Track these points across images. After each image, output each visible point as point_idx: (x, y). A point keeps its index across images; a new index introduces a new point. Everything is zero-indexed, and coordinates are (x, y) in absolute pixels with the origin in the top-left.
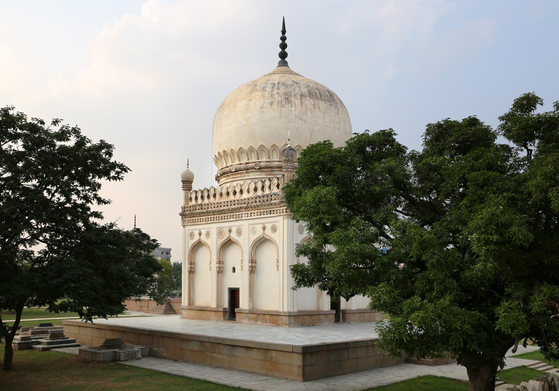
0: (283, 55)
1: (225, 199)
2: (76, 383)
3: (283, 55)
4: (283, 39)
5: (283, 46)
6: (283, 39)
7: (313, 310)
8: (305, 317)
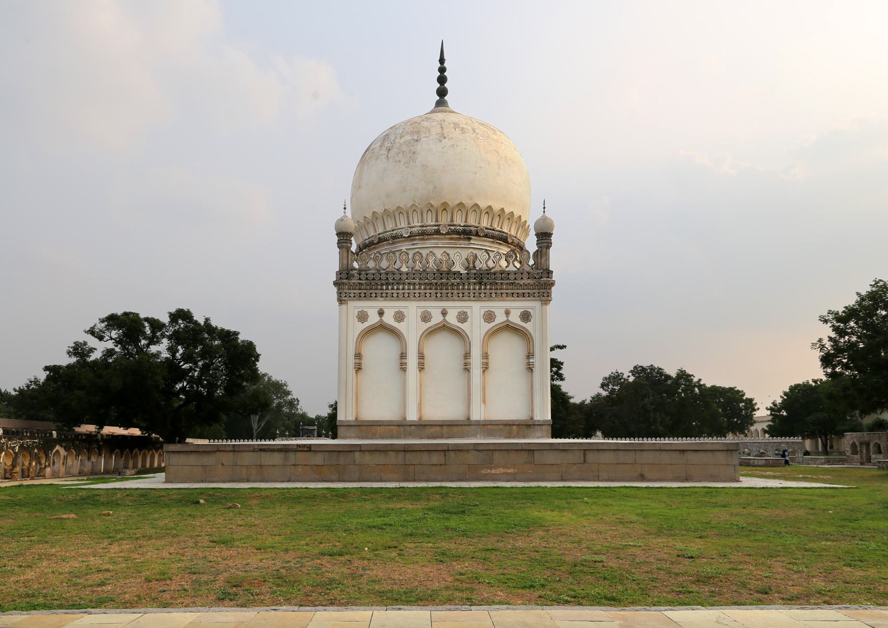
0: (442, 92)
1: (521, 291)
2: (493, 471)
3: (442, 92)
4: (442, 70)
5: (442, 80)
6: (442, 70)
7: (384, 419)
8: (392, 427)
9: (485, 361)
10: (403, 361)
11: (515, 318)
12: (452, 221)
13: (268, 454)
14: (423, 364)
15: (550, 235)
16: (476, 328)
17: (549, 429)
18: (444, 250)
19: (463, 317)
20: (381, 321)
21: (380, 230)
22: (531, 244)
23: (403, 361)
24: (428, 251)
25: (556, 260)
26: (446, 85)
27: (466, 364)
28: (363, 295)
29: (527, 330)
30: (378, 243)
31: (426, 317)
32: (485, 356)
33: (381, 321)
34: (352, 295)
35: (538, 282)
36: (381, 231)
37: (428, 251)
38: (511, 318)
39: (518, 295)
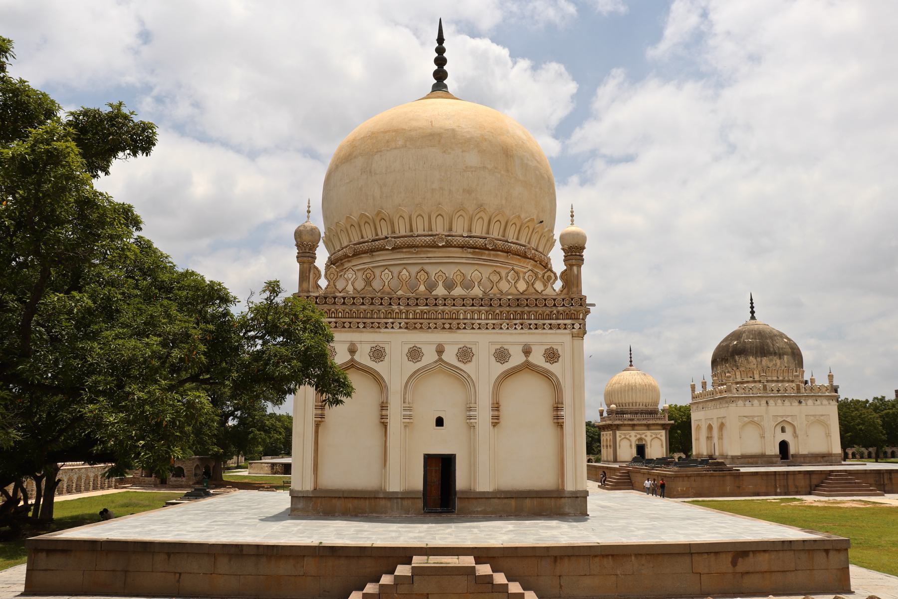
9: (496, 413)
10: (384, 413)
11: (537, 358)
12: (450, 230)
13: (762, 554)
14: (497, 417)
15: (583, 248)
16: (484, 370)
17: (420, 504)
18: (495, 268)
19: (378, 354)
20: (352, 360)
21: (356, 239)
22: (557, 261)
23: (384, 413)
24: (418, 268)
25: (590, 282)
26: (445, 68)
27: (383, 417)
28: (361, 326)
29: (553, 374)
30: (354, 255)
31: (415, 354)
32: (496, 407)
33: (352, 360)
34: (447, 326)
35: (571, 309)
36: (356, 240)
37: (418, 268)
38: (533, 359)
39: (551, 327)
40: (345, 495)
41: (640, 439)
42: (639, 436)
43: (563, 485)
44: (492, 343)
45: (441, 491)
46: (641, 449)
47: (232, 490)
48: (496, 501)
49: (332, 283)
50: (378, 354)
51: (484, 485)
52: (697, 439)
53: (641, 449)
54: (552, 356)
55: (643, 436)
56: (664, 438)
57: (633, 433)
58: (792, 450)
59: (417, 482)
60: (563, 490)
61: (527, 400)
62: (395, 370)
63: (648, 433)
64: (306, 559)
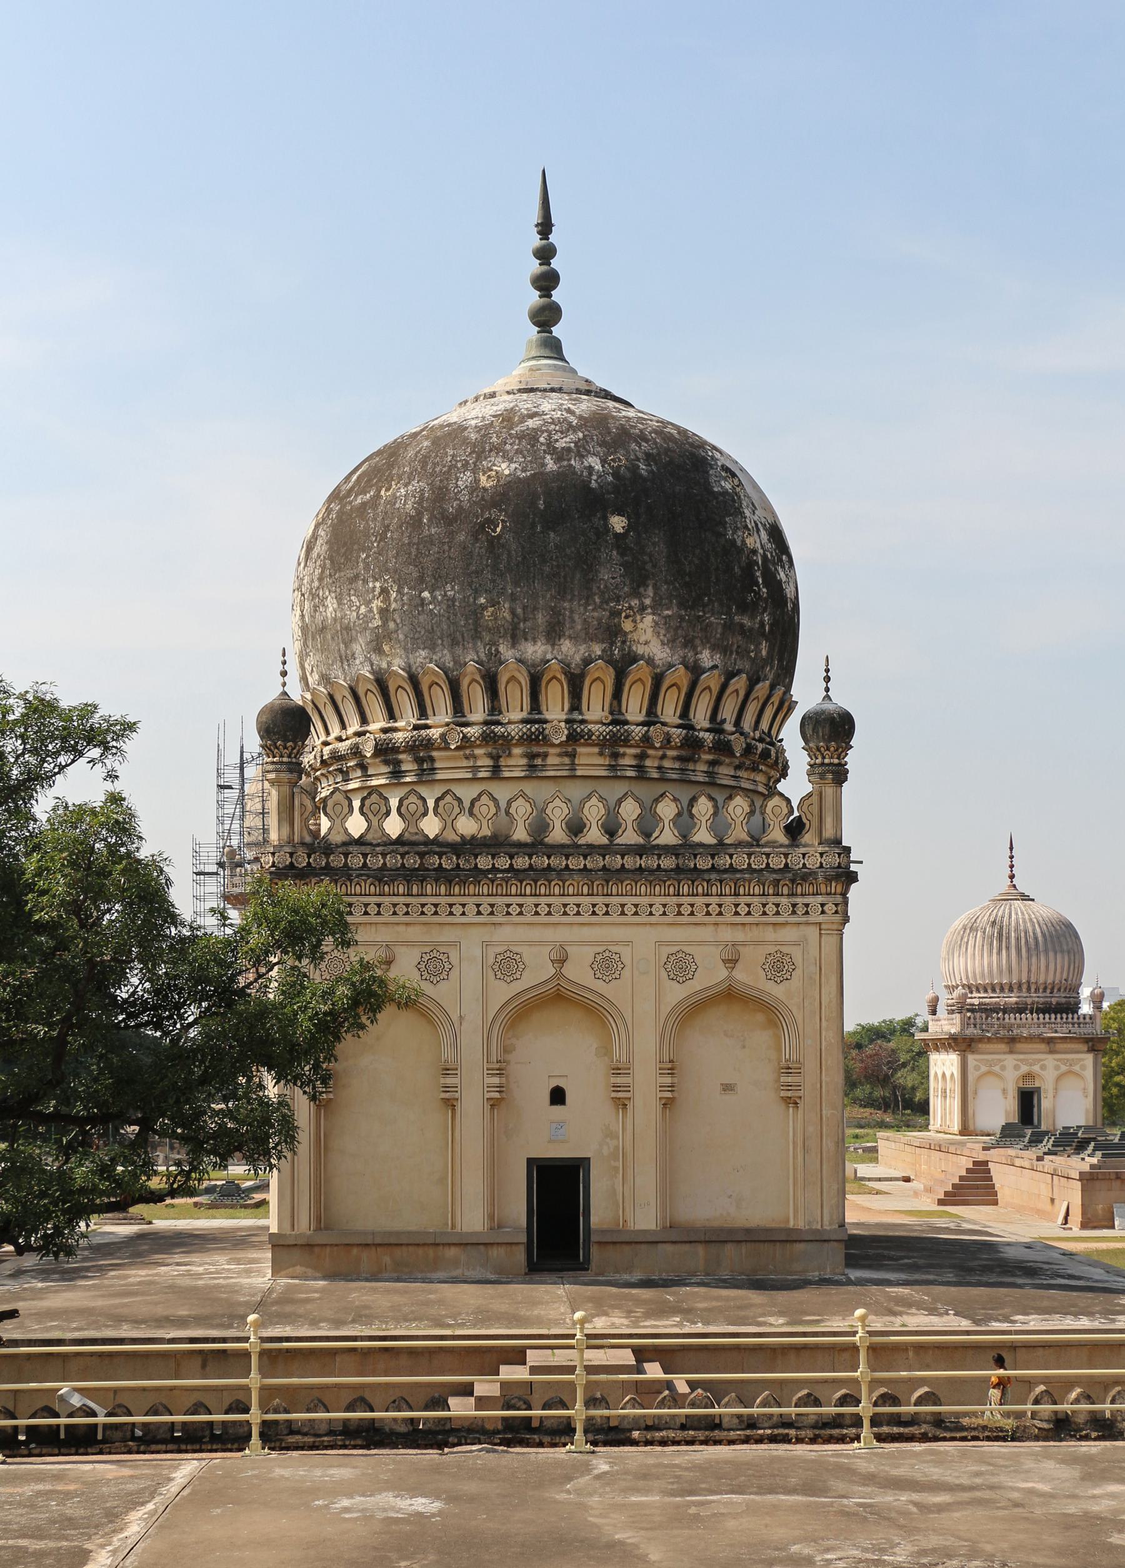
17: (520, 1256)
19: (435, 966)
38: (741, 975)
40: (378, 1241)
41: (1029, 1076)
42: (1024, 1069)
43: (349, 835)
44: (660, 943)
45: (557, 1225)
46: (1027, 1100)
47: (774, 1225)
48: (669, 1248)
49: (338, 821)
50: (607, 965)
51: (645, 1219)
52: (374, 1290)
53: (1027, 1100)
54: (779, 967)
55: (1036, 1068)
56: (1089, 1073)
57: (1010, 1060)
58: (603, 1206)
59: (517, 1208)
60: (508, 837)
61: (729, 1055)
62: (469, 994)
63: (1050, 1060)
64: (338, 1359)
